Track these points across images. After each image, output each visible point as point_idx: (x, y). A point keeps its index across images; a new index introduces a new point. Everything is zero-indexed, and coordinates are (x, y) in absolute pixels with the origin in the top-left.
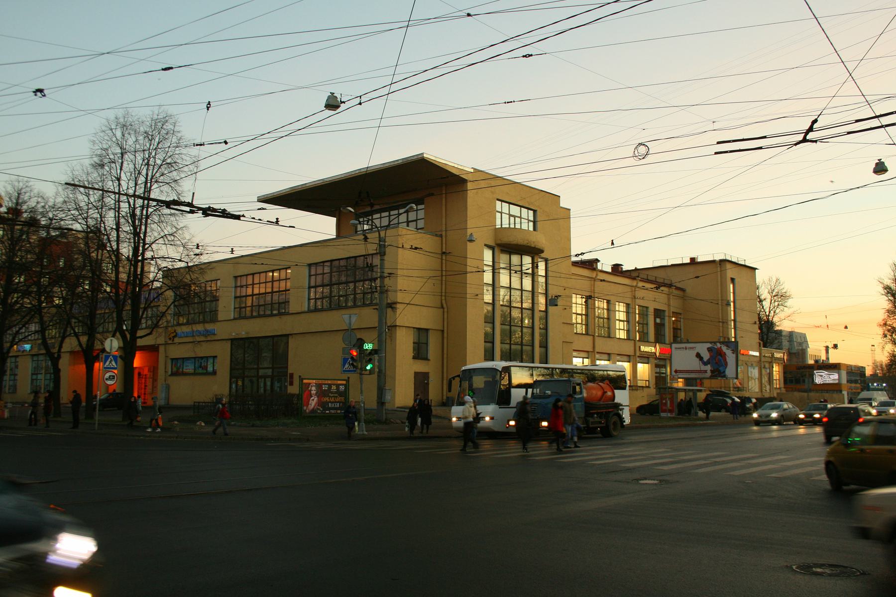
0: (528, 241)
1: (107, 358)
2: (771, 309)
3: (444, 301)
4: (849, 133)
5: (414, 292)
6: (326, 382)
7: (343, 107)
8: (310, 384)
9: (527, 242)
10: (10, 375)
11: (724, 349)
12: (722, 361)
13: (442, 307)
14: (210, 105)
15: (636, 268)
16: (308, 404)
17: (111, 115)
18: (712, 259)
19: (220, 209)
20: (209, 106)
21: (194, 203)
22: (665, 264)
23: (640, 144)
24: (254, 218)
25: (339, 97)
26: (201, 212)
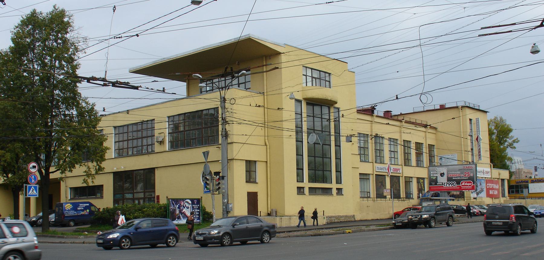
3: (267, 141)
9: (326, 96)
13: (266, 145)
14: (115, 8)
18: (456, 106)
19: (100, 78)
20: (114, 9)
21: (107, 78)
24: (148, 88)
26: (86, 80)
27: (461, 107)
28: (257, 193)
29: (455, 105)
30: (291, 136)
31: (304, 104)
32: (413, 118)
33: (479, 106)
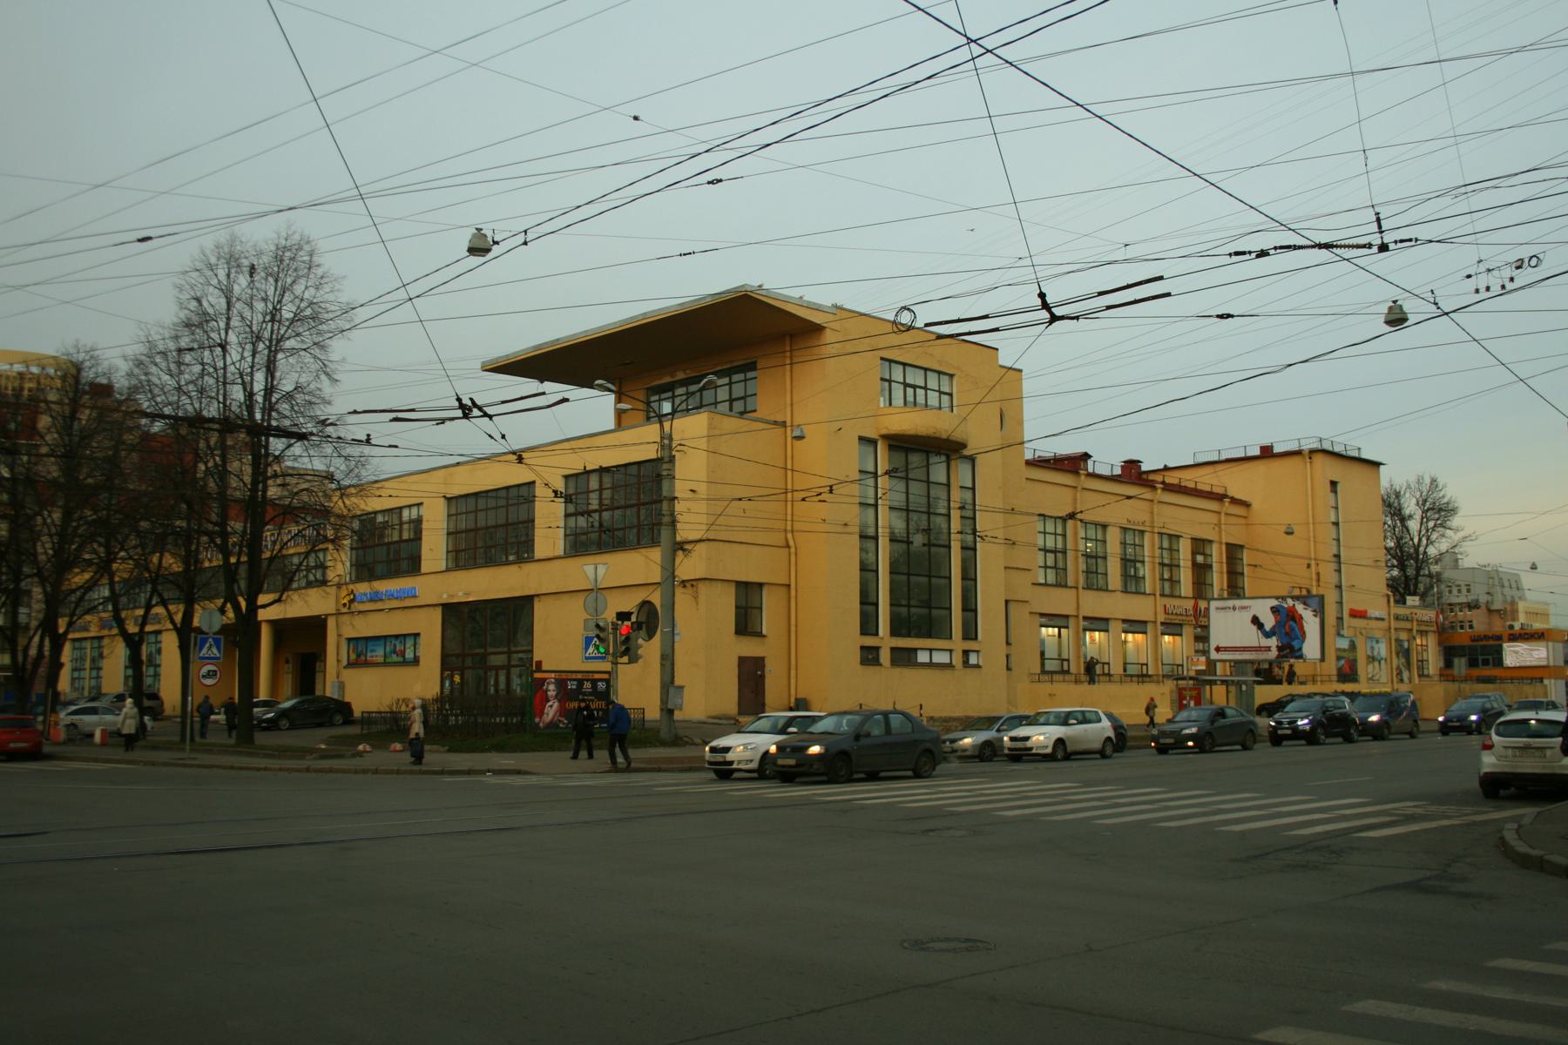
0: (936, 429)
1: (204, 642)
2: (1422, 533)
4: (1109, 308)
5: (717, 528)
6: (574, 676)
7: (496, 250)
8: (545, 679)
9: (934, 430)
10: (91, 669)
11: (1300, 608)
12: (1297, 629)
13: (788, 546)
15: (1165, 466)
16: (541, 713)
17: (208, 242)
18: (1244, 455)
22: (1216, 459)
23: (905, 308)
25: (489, 234)
27: (1307, 451)
28: (763, 659)
29: (1293, 447)
30: (846, 525)
32: (1188, 479)
33: (1359, 449)
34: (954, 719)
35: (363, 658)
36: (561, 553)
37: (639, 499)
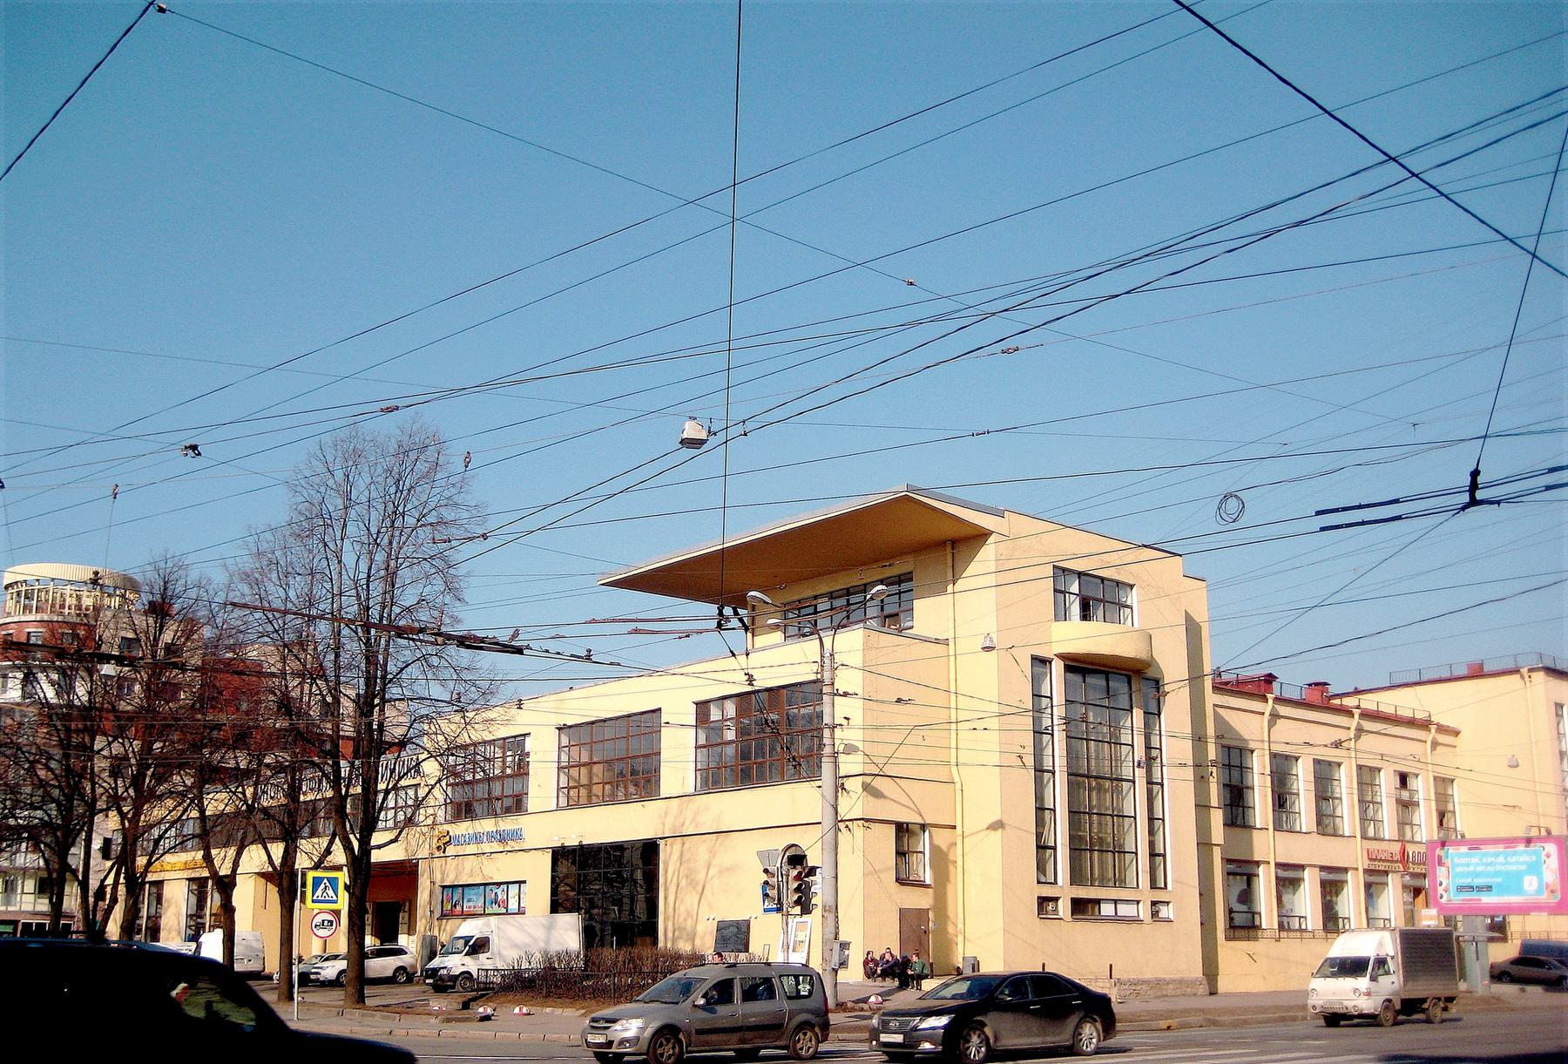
4: (1549, 488)
24: (547, 651)
28: (1072, 899)
31: (1058, 667)
34: (1144, 982)
35: (459, 908)
36: (691, 790)
37: (628, 733)
